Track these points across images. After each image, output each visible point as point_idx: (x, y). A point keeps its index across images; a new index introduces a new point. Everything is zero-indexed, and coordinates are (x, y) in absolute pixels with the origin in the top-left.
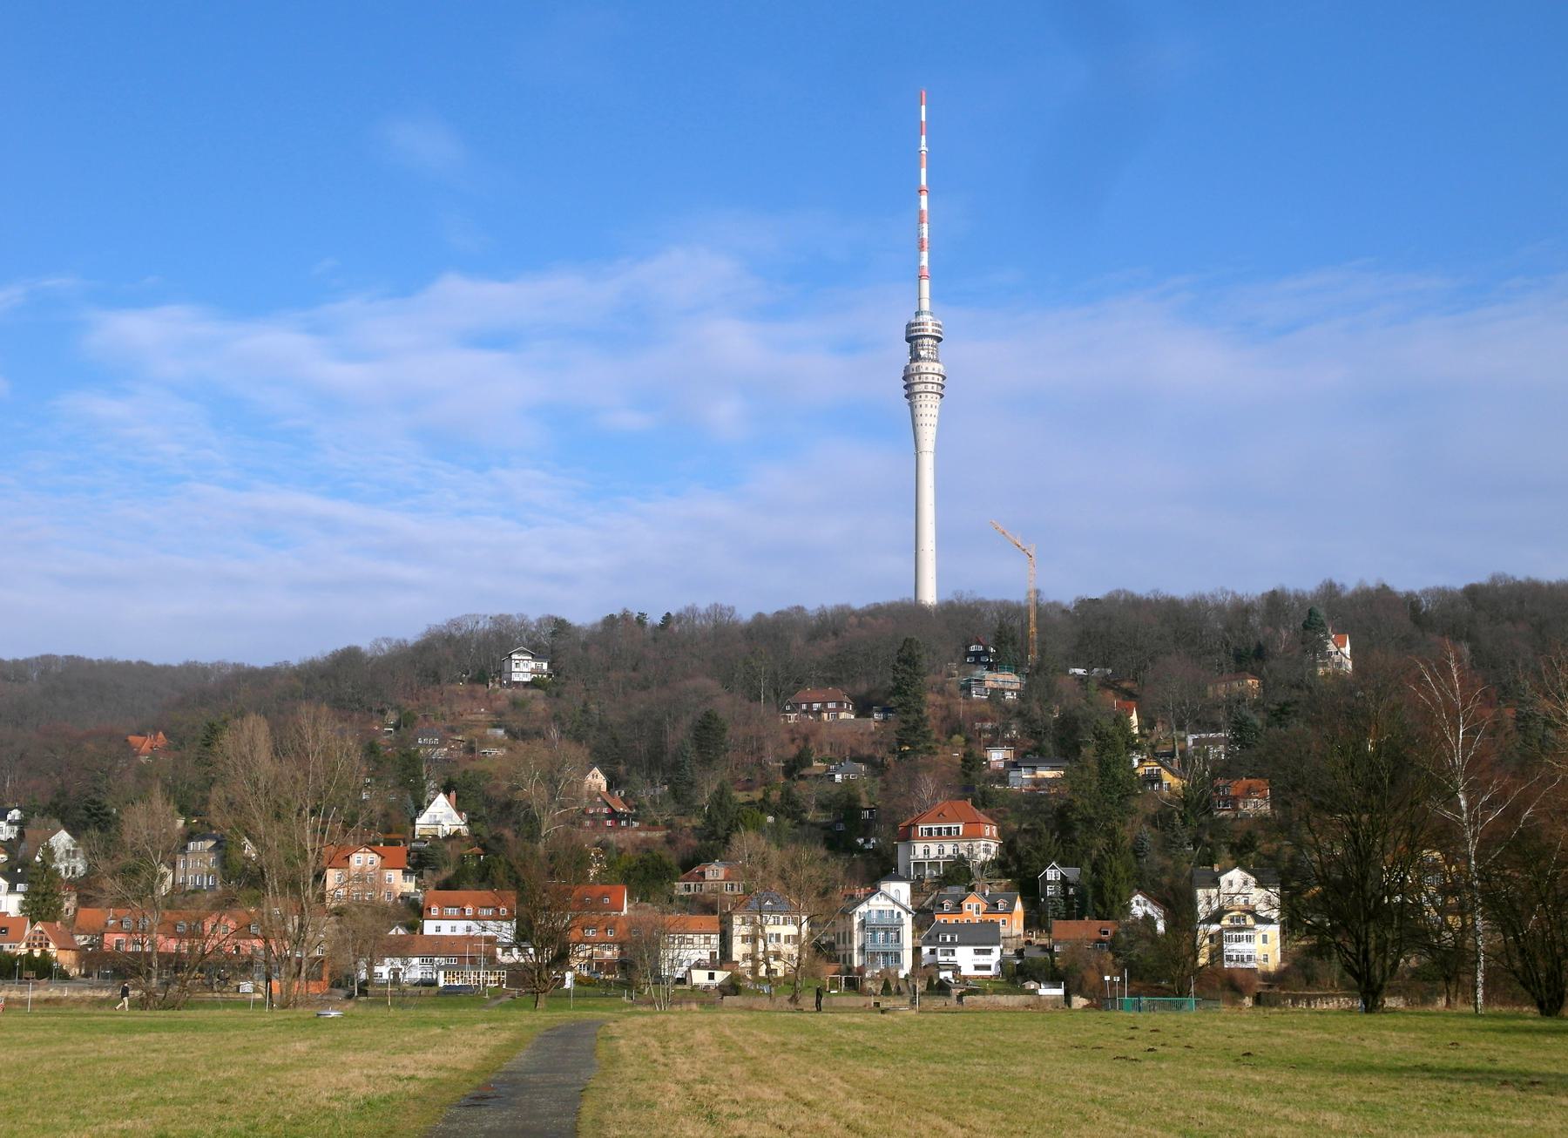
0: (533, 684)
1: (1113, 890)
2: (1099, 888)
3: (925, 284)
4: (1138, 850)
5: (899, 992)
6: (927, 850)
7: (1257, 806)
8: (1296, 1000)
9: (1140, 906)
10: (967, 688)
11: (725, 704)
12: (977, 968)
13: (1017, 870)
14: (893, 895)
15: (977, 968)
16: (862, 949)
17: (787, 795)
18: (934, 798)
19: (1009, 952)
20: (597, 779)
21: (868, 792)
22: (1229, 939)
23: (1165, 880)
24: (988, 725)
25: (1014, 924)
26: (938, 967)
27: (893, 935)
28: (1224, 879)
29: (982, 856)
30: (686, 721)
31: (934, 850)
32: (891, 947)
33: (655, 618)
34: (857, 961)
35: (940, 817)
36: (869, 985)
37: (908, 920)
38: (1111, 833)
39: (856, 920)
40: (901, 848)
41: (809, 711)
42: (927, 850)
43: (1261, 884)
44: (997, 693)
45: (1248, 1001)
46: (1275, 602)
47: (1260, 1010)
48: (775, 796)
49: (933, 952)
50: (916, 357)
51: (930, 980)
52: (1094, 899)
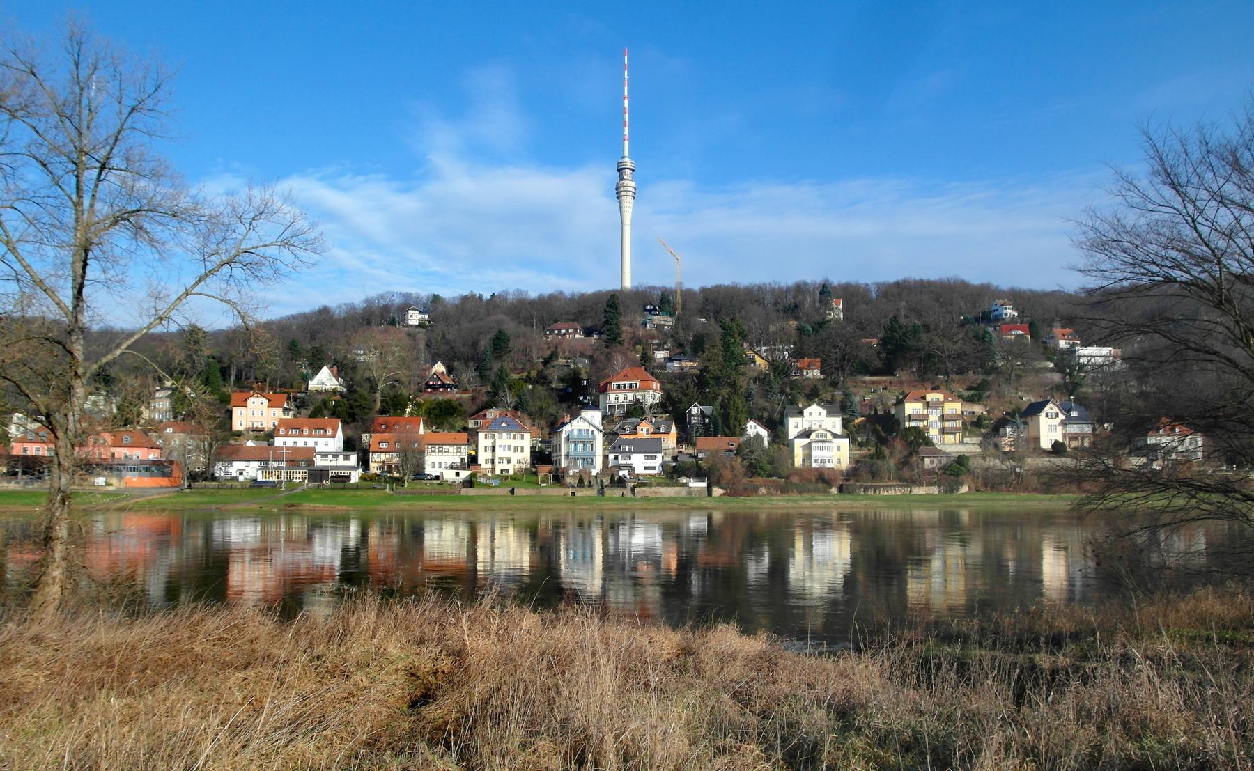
0: (420, 326)
1: (736, 419)
2: (726, 417)
3: (627, 143)
4: (748, 397)
5: (590, 485)
6: (617, 398)
7: (814, 373)
8: (866, 489)
9: (754, 428)
10: (645, 324)
11: (510, 327)
12: (646, 468)
13: (673, 408)
14: (590, 419)
15: (646, 468)
16: (567, 456)
17: (540, 373)
18: (622, 368)
19: (668, 458)
20: (439, 368)
21: (583, 366)
22: (816, 448)
23: (765, 414)
24: (656, 341)
25: (670, 440)
26: (619, 467)
27: (588, 446)
28: (806, 412)
29: (650, 401)
30: (490, 336)
31: (621, 397)
32: (588, 454)
33: (487, 296)
34: (564, 464)
35: (626, 377)
36: (569, 480)
37: (599, 438)
38: (733, 384)
39: (563, 436)
40: (601, 397)
41: (559, 334)
42: (617, 398)
43: (830, 414)
44: (660, 327)
45: (834, 490)
46: (800, 288)
47: (843, 496)
48: (534, 374)
49: (616, 458)
50: (622, 179)
51: (613, 477)
52: (725, 424)
